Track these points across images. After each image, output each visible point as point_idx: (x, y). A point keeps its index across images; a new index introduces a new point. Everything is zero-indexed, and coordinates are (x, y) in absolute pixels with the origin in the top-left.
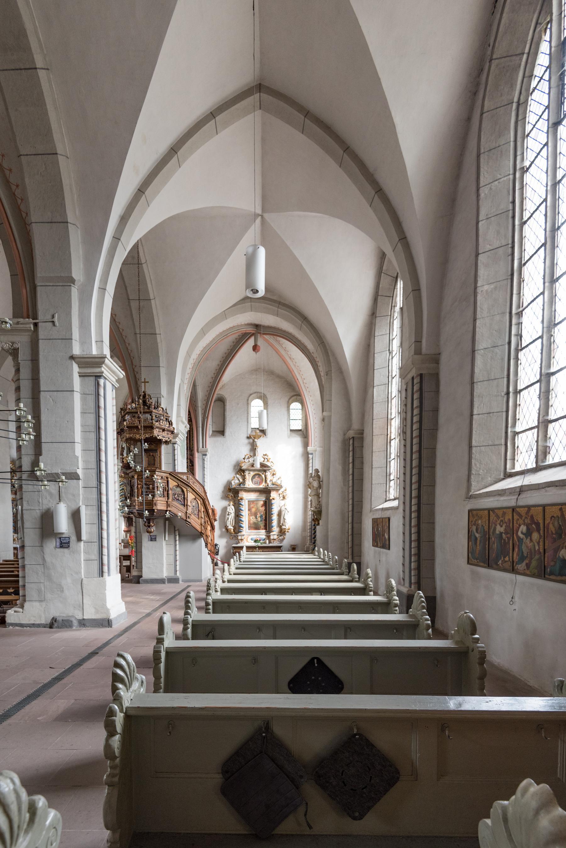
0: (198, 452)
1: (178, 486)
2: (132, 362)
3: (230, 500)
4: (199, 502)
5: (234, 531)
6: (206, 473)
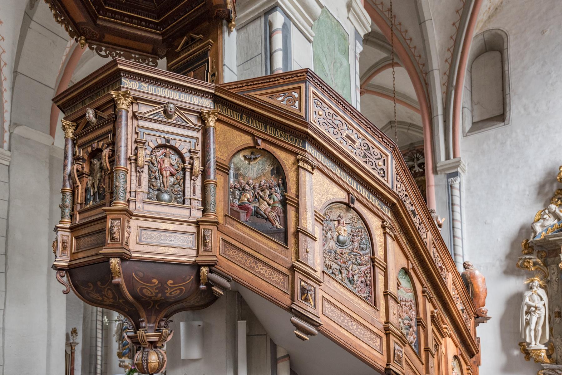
0: (435, 172)
1: (253, 151)
3: (531, 275)
4: (374, 223)
5: (549, 356)
6: (457, 216)
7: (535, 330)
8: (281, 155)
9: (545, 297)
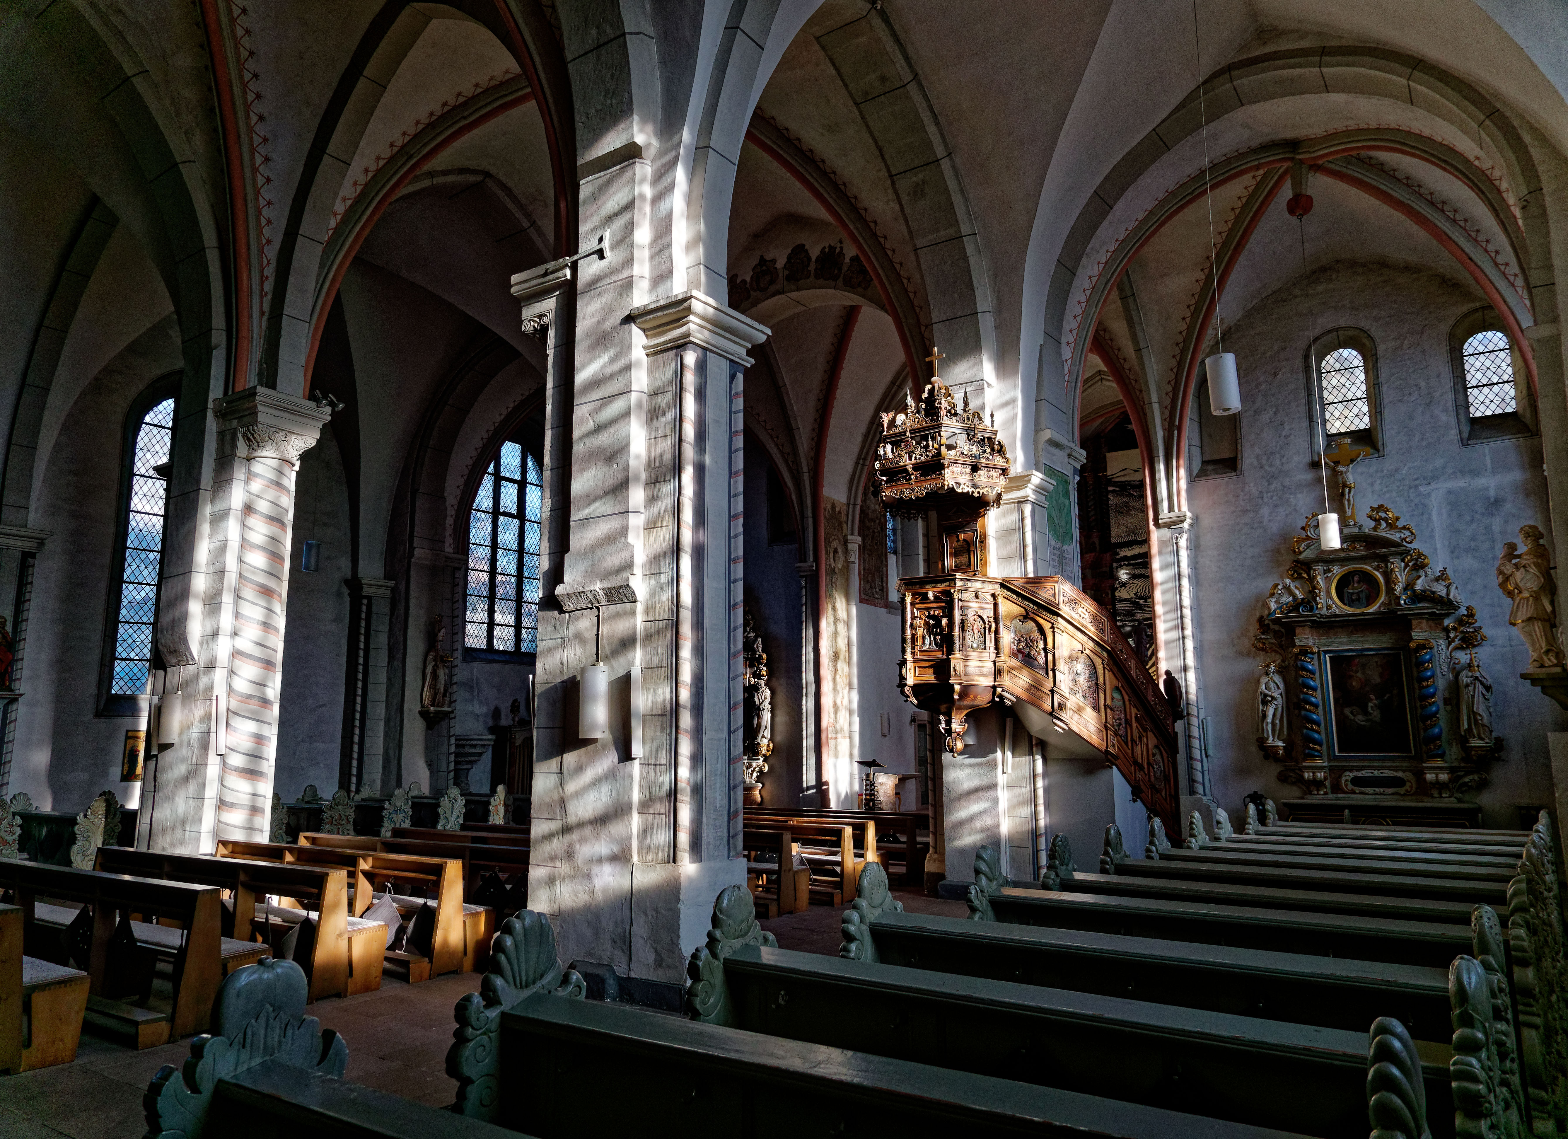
0: (1157, 525)
2: (918, 319)
7: (1273, 723)
8: (1041, 621)
9: (1281, 685)
